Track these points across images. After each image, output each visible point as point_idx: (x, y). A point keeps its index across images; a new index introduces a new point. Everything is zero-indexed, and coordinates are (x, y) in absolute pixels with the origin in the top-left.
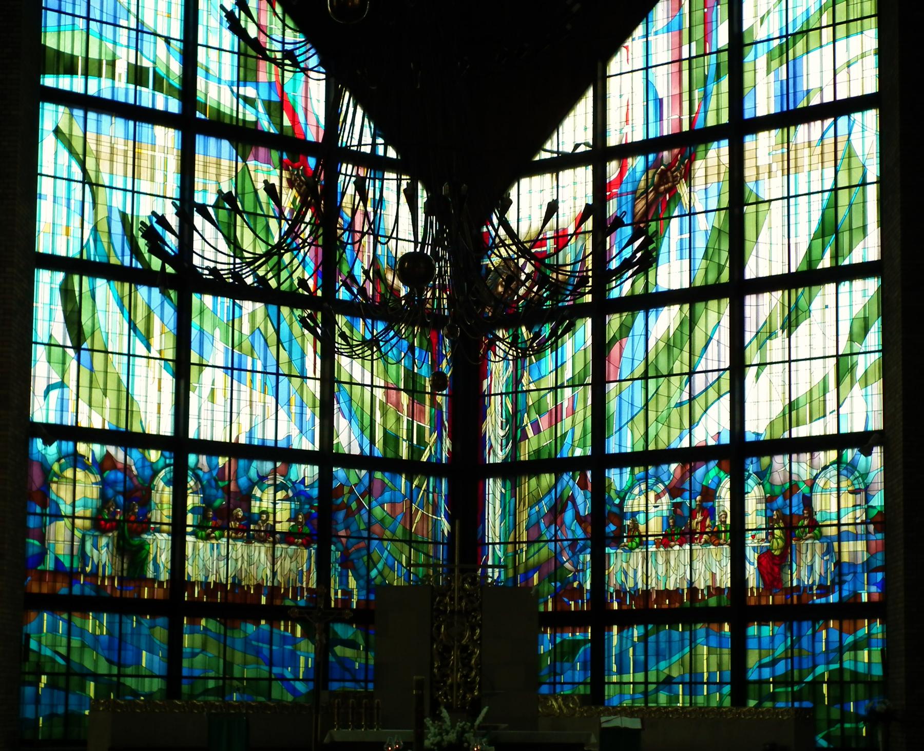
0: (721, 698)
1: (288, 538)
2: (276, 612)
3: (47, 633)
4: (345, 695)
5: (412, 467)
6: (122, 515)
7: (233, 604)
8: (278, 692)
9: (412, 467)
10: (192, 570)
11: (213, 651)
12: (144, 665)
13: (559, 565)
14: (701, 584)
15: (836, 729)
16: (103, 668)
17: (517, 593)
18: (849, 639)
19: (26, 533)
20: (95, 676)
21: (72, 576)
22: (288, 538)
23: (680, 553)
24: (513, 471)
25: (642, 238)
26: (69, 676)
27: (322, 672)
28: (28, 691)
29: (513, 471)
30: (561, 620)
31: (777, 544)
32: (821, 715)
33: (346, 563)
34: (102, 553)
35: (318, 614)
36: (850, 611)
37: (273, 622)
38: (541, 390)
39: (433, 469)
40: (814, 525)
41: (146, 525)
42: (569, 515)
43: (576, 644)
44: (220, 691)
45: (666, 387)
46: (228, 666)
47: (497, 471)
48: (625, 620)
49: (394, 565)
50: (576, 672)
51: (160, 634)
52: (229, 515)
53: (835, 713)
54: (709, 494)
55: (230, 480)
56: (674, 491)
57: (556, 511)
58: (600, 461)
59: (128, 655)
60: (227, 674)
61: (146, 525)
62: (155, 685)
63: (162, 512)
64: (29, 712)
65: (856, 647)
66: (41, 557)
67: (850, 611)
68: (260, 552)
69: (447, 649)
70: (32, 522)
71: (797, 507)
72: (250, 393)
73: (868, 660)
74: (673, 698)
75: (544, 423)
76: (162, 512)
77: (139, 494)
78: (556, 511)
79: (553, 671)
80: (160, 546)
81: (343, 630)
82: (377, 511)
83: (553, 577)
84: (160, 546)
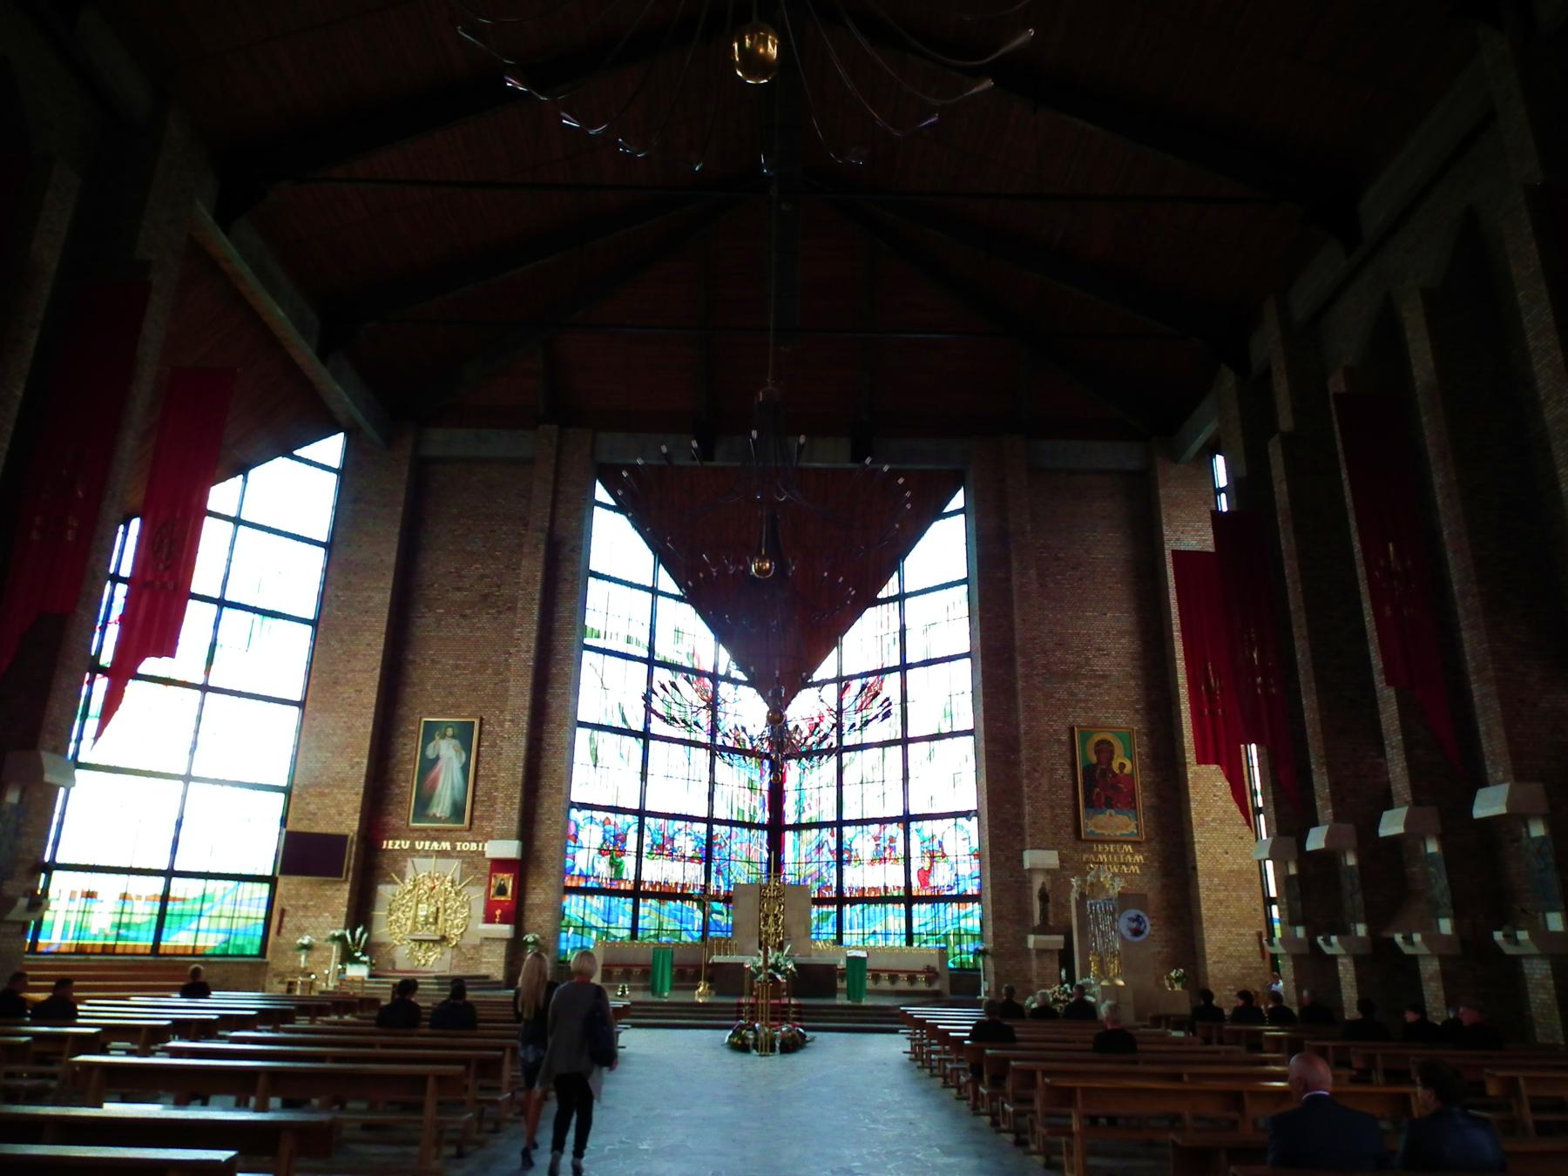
0: (900, 942)
1: (691, 859)
2: (684, 897)
3: (574, 906)
4: (718, 938)
5: (750, 826)
6: (613, 849)
7: (665, 894)
8: (685, 937)
9: (750, 826)
10: (645, 876)
11: (654, 916)
12: (738, 464)
13: (820, 874)
14: (890, 885)
15: (957, 959)
16: (600, 924)
17: (801, 888)
18: (962, 912)
19: (565, 855)
20: (596, 928)
21: (587, 877)
22: (691, 859)
23: (879, 867)
24: (798, 827)
25: (232, 1153)
26: (584, 927)
27: (705, 927)
28: (563, 935)
29: (798, 827)
30: (820, 901)
31: (926, 866)
32: (950, 951)
33: (718, 872)
34: (603, 867)
35: (704, 898)
36: (962, 898)
37: (930, 1037)
38: (810, 790)
39: (760, 826)
40: (944, 856)
41: (623, 852)
42: (825, 850)
43: (829, 914)
44: (657, 936)
45: (872, 785)
46: (661, 924)
47: (790, 827)
48: (853, 901)
49: (742, 874)
50: (829, 928)
51: (629, 907)
52: (664, 848)
53: (957, 950)
54: (892, 840)
55: (502, 1048)
56: (876, 838)
57: (819, 848)
58: (840, 823)
59: (613, 917)
60: (660, 929)
61: (623, 852)
62: (626, 933)
63: (631, 844)
64: (563, 946)
65: (966, 916)
66: (573, 868)
67: (962, 898)
68: (678, 865)
69: (767, 916)
70: (570, 850)
71: (936, 847)
72: (678, 781)
73: (973, 924)
74: (877, 941)
75: (813, 804)
76: (631, 844)
77: (620, 838)
78: (819, 848)
79: (818, 927)
80: (629, 863)
81: (717, 906)
82: (734, 848)
83: (818, 880)
84: (629, 863)
